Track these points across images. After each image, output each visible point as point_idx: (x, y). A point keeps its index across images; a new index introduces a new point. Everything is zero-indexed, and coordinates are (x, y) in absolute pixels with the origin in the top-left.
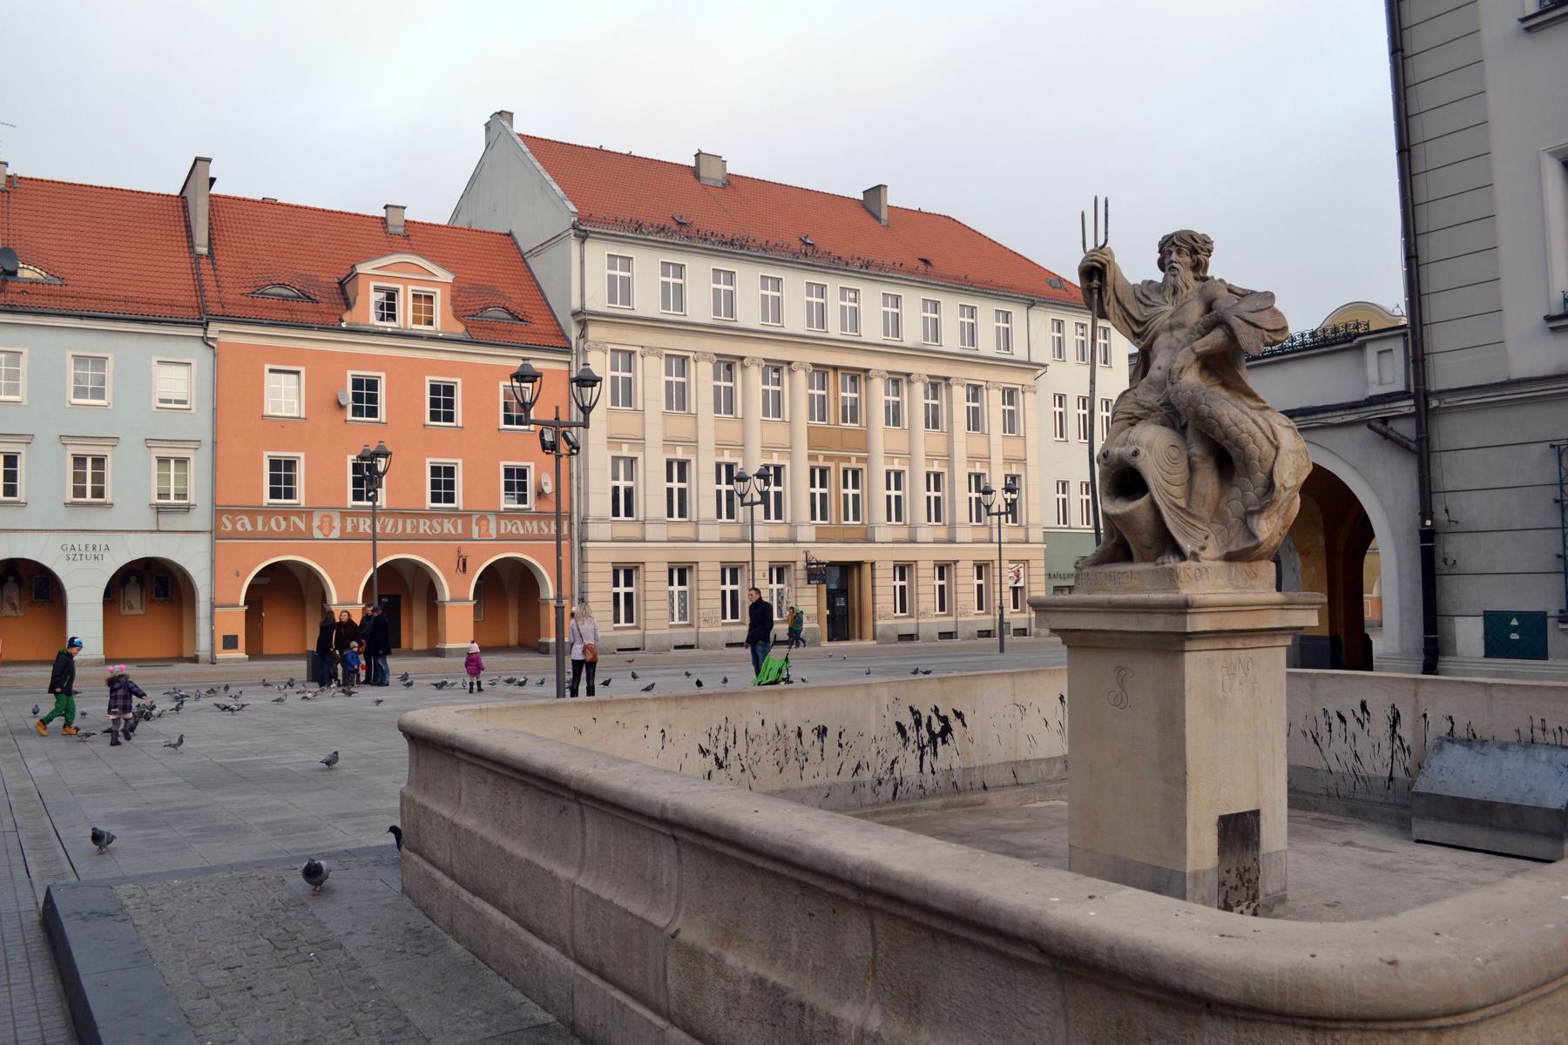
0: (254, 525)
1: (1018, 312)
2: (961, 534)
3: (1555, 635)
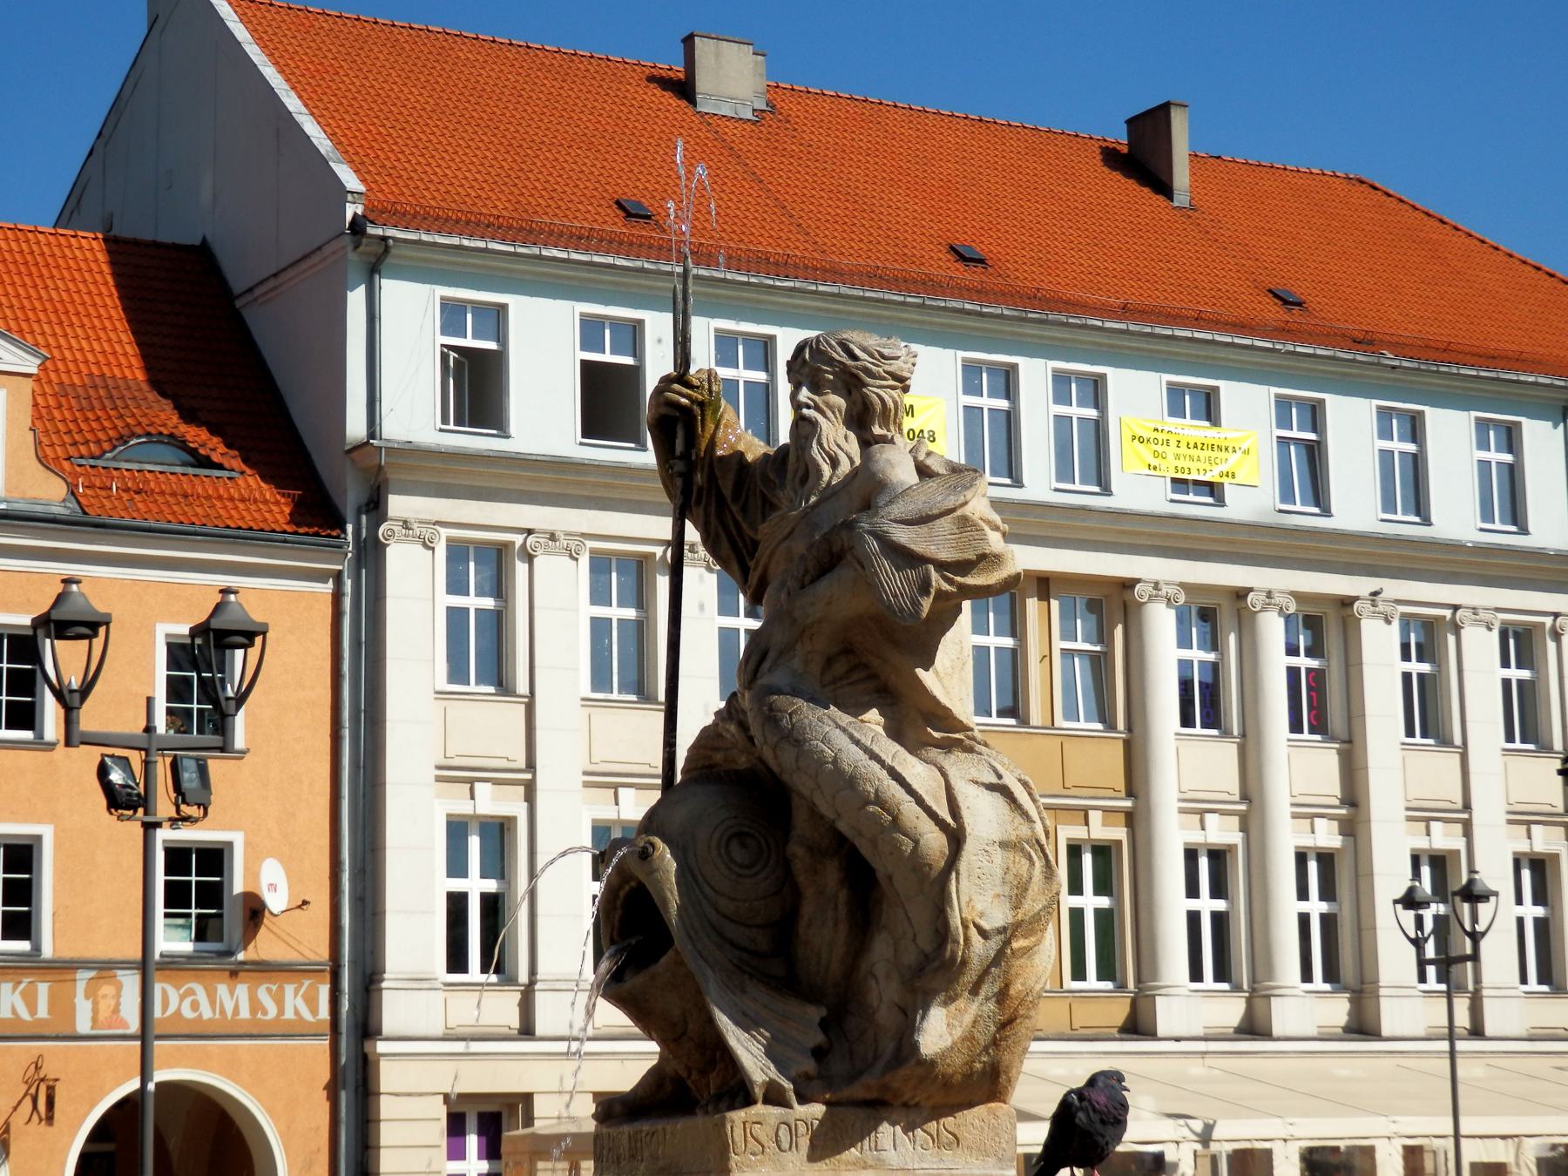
2: (552, 1013)
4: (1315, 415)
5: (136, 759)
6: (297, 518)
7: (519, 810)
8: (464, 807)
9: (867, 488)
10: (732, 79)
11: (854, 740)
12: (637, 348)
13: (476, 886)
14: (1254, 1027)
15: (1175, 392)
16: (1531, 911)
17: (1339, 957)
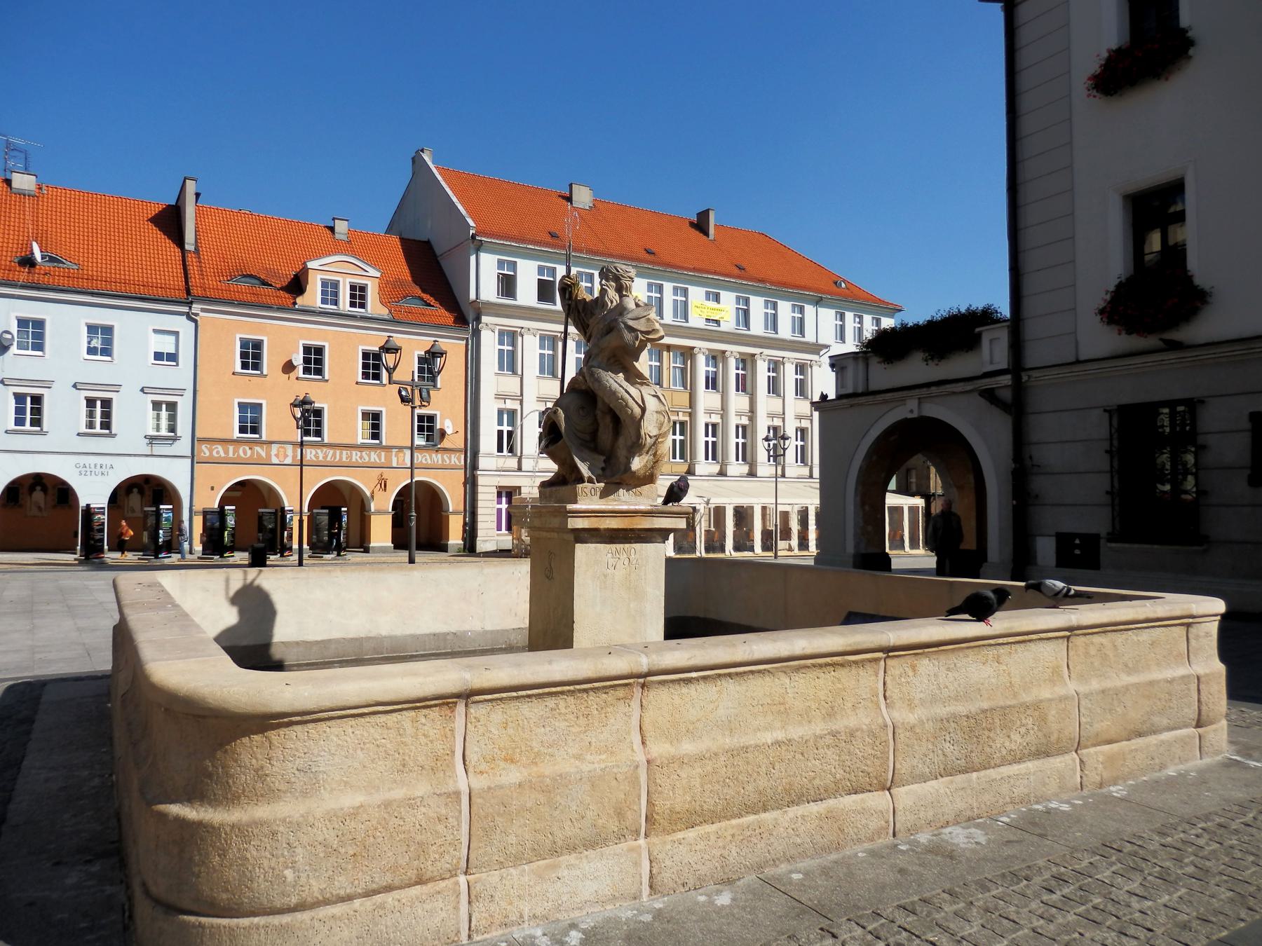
0: (226, 452)
1: (809, 310)
2: (527, 465)
3: (1108, 550)
4: (747, 301)
5: (409, 388)
6: (455, 322)
7: (518, 408)
8: (503, 406)
9: (621, 309)
10: (583, 197)
11: (615, 381)
12: (554, 275)
13: (506, 428)
14: (722, 473)
15: (708, 294)
16: (800, 443)
17: (746, 454)
